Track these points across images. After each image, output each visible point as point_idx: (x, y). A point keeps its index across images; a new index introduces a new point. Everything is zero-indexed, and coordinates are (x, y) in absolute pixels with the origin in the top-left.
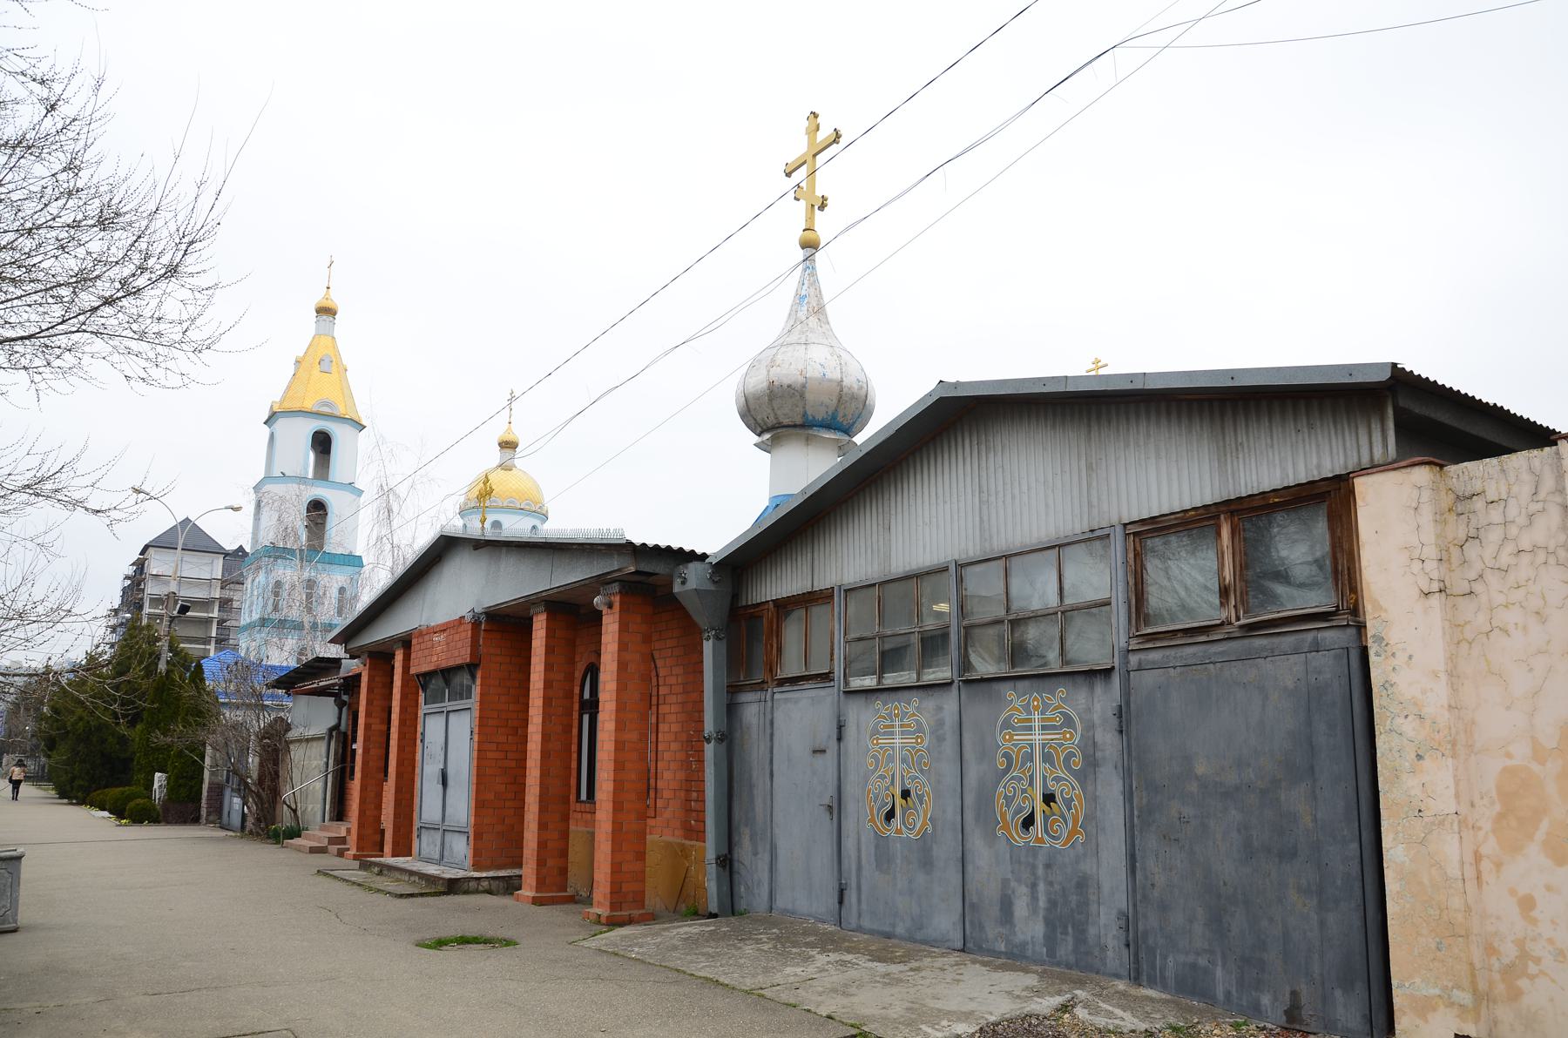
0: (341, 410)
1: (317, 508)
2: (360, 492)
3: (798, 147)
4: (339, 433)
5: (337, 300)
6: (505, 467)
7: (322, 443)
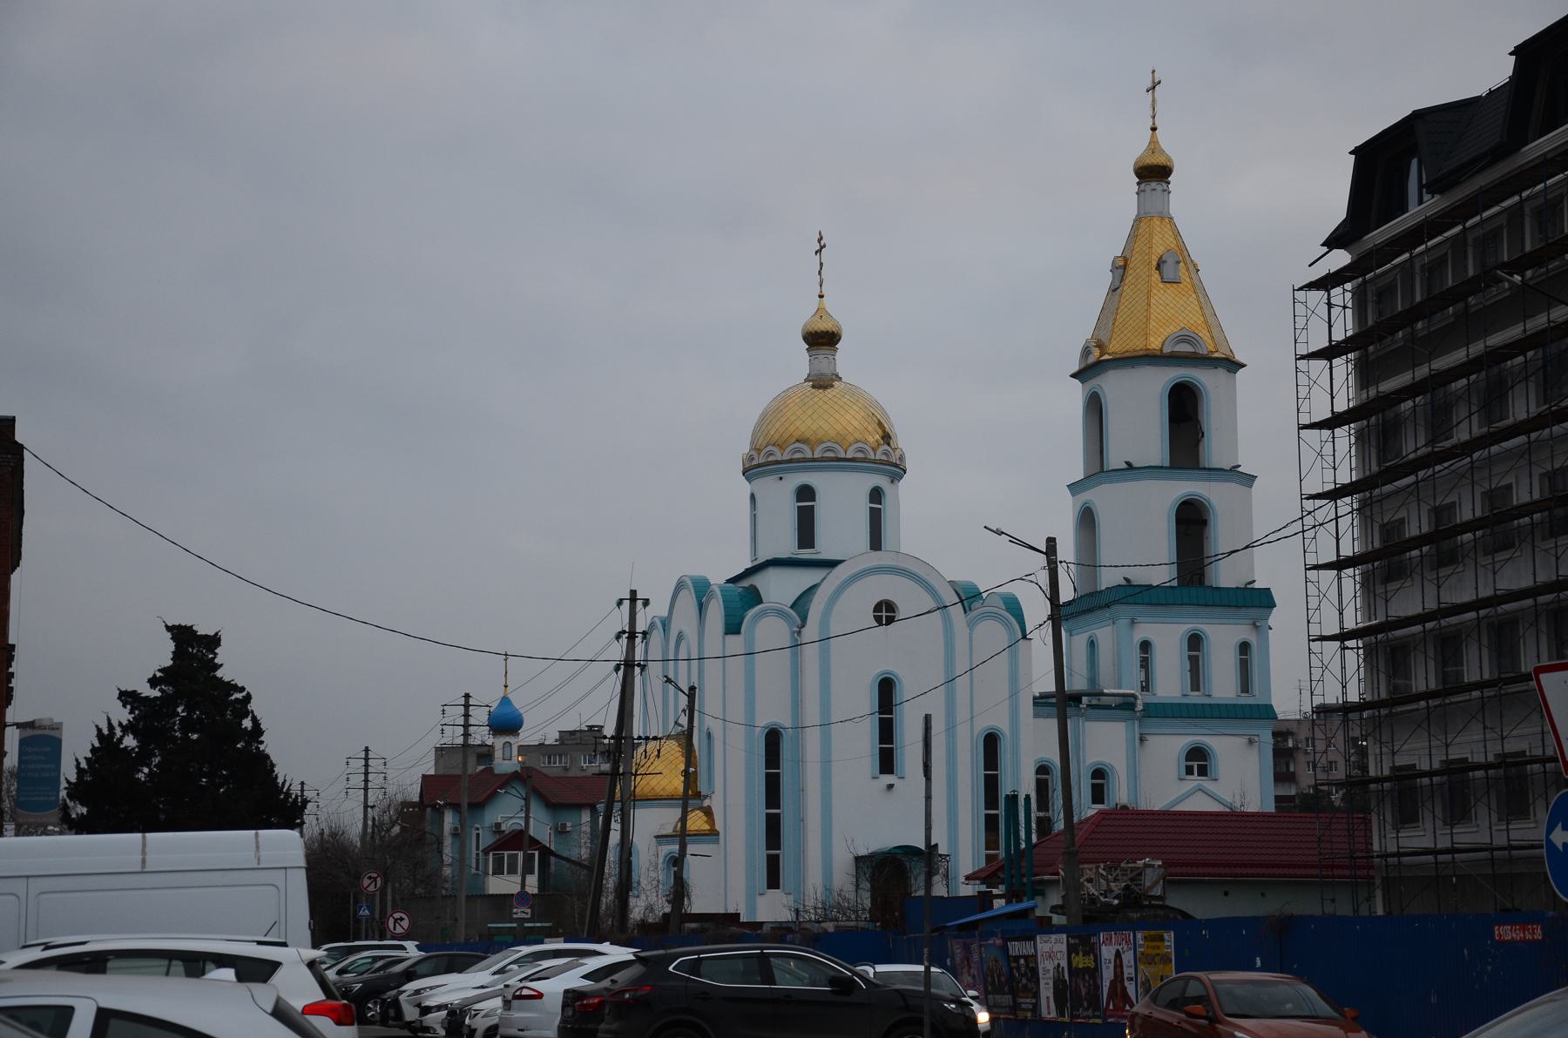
0: (1207, 346)
1: (1192, 521)
2: (1249, 480)
3: (1150, 85)
4: (1204, 378)
5: (1173, 148)
6: (822, 382)
7: (1184, 408)
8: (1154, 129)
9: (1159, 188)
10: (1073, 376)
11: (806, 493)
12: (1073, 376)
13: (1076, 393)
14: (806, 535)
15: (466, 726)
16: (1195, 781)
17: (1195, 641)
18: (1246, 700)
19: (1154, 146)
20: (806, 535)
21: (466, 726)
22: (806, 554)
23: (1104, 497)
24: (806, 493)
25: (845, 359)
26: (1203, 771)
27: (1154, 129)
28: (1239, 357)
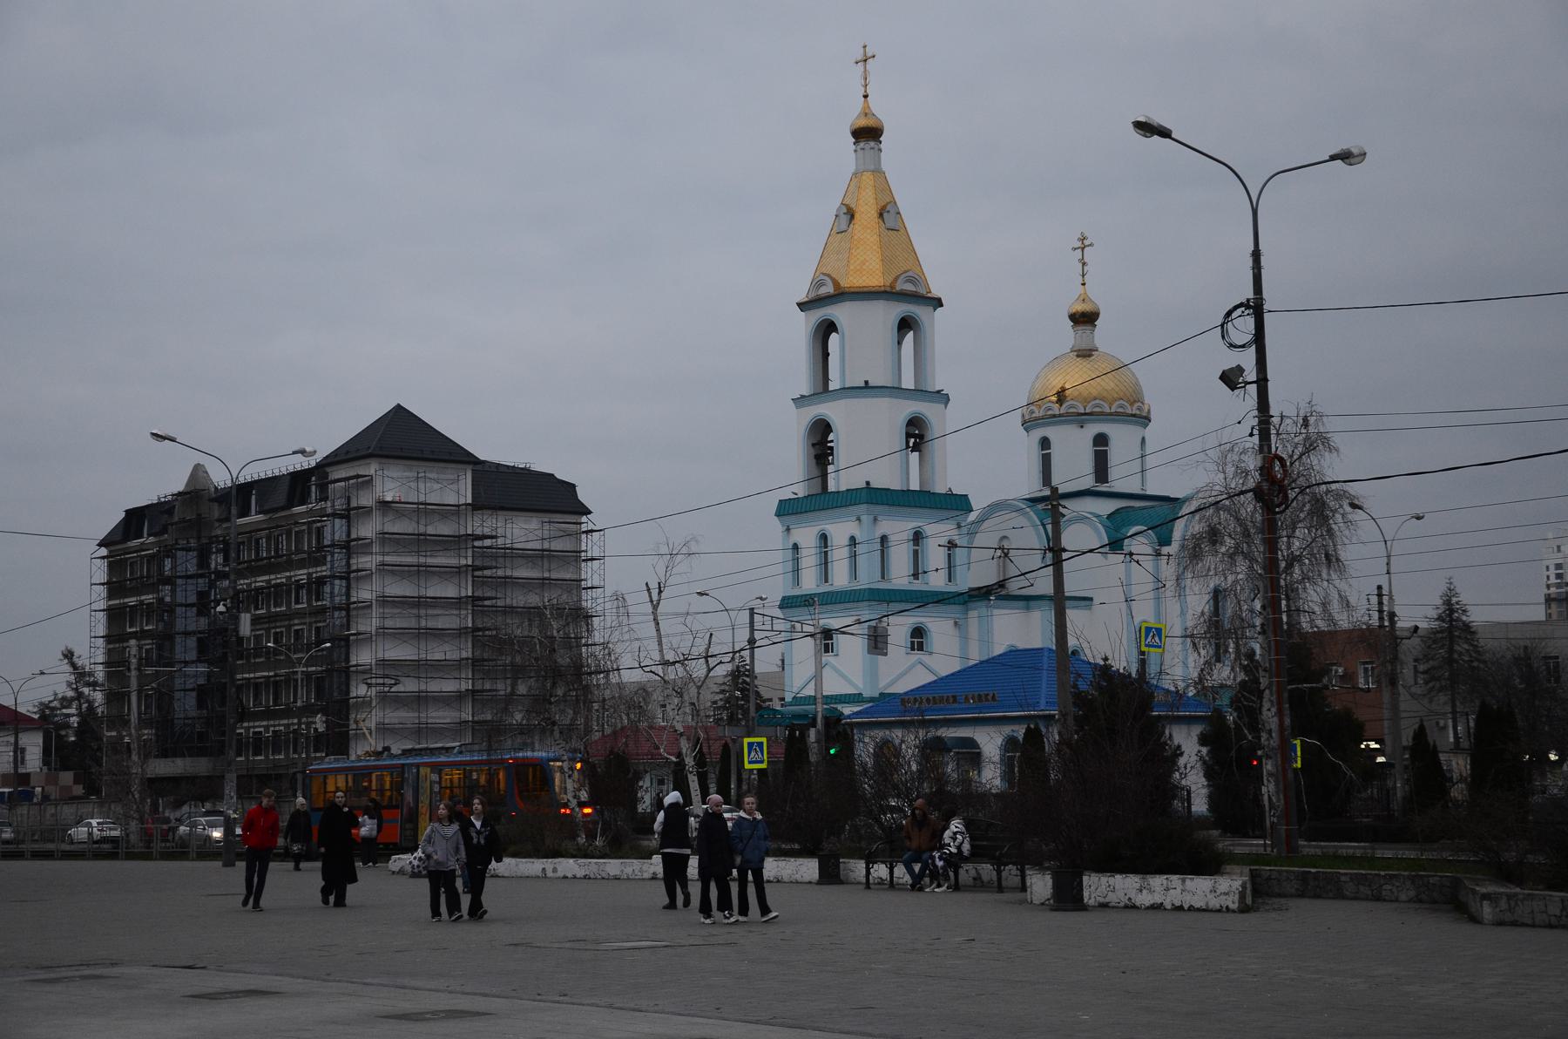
5: (883, 112)
8: (866, 97)
9: (872, 144)
10: (799, 305)
11: (1101, 440)
12: (802, 306)
13: (802, 326)
14: (1101, 471)
15: (187, 606)
16: (917, 656)
17: (918, 537)
18: (825, 588)
19: (866, 113)
20: (1101, 471)
21: (187, 606)
22: (1103, 488)
23: (830, 410)
24: (1101, 440)
25: (1102, 334)
26: (921, 648)
27: (866, 97)
28: (936, 291)
